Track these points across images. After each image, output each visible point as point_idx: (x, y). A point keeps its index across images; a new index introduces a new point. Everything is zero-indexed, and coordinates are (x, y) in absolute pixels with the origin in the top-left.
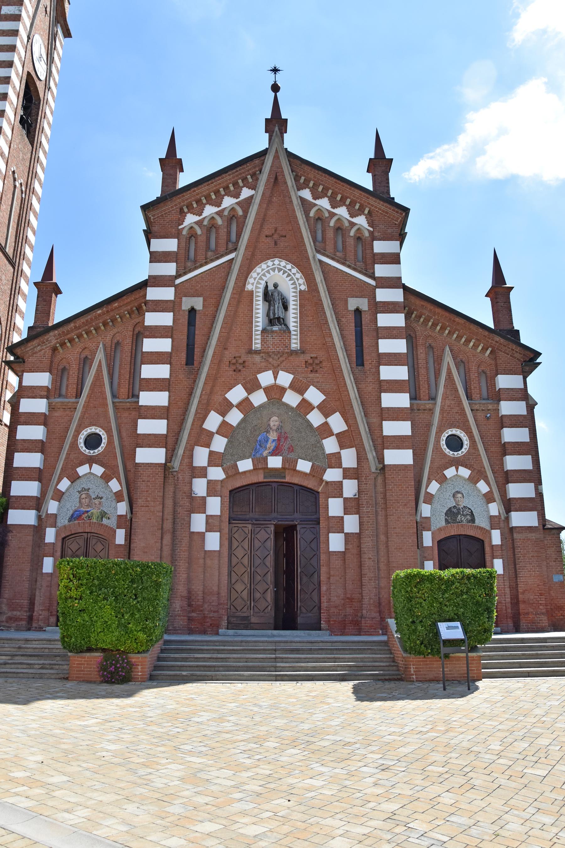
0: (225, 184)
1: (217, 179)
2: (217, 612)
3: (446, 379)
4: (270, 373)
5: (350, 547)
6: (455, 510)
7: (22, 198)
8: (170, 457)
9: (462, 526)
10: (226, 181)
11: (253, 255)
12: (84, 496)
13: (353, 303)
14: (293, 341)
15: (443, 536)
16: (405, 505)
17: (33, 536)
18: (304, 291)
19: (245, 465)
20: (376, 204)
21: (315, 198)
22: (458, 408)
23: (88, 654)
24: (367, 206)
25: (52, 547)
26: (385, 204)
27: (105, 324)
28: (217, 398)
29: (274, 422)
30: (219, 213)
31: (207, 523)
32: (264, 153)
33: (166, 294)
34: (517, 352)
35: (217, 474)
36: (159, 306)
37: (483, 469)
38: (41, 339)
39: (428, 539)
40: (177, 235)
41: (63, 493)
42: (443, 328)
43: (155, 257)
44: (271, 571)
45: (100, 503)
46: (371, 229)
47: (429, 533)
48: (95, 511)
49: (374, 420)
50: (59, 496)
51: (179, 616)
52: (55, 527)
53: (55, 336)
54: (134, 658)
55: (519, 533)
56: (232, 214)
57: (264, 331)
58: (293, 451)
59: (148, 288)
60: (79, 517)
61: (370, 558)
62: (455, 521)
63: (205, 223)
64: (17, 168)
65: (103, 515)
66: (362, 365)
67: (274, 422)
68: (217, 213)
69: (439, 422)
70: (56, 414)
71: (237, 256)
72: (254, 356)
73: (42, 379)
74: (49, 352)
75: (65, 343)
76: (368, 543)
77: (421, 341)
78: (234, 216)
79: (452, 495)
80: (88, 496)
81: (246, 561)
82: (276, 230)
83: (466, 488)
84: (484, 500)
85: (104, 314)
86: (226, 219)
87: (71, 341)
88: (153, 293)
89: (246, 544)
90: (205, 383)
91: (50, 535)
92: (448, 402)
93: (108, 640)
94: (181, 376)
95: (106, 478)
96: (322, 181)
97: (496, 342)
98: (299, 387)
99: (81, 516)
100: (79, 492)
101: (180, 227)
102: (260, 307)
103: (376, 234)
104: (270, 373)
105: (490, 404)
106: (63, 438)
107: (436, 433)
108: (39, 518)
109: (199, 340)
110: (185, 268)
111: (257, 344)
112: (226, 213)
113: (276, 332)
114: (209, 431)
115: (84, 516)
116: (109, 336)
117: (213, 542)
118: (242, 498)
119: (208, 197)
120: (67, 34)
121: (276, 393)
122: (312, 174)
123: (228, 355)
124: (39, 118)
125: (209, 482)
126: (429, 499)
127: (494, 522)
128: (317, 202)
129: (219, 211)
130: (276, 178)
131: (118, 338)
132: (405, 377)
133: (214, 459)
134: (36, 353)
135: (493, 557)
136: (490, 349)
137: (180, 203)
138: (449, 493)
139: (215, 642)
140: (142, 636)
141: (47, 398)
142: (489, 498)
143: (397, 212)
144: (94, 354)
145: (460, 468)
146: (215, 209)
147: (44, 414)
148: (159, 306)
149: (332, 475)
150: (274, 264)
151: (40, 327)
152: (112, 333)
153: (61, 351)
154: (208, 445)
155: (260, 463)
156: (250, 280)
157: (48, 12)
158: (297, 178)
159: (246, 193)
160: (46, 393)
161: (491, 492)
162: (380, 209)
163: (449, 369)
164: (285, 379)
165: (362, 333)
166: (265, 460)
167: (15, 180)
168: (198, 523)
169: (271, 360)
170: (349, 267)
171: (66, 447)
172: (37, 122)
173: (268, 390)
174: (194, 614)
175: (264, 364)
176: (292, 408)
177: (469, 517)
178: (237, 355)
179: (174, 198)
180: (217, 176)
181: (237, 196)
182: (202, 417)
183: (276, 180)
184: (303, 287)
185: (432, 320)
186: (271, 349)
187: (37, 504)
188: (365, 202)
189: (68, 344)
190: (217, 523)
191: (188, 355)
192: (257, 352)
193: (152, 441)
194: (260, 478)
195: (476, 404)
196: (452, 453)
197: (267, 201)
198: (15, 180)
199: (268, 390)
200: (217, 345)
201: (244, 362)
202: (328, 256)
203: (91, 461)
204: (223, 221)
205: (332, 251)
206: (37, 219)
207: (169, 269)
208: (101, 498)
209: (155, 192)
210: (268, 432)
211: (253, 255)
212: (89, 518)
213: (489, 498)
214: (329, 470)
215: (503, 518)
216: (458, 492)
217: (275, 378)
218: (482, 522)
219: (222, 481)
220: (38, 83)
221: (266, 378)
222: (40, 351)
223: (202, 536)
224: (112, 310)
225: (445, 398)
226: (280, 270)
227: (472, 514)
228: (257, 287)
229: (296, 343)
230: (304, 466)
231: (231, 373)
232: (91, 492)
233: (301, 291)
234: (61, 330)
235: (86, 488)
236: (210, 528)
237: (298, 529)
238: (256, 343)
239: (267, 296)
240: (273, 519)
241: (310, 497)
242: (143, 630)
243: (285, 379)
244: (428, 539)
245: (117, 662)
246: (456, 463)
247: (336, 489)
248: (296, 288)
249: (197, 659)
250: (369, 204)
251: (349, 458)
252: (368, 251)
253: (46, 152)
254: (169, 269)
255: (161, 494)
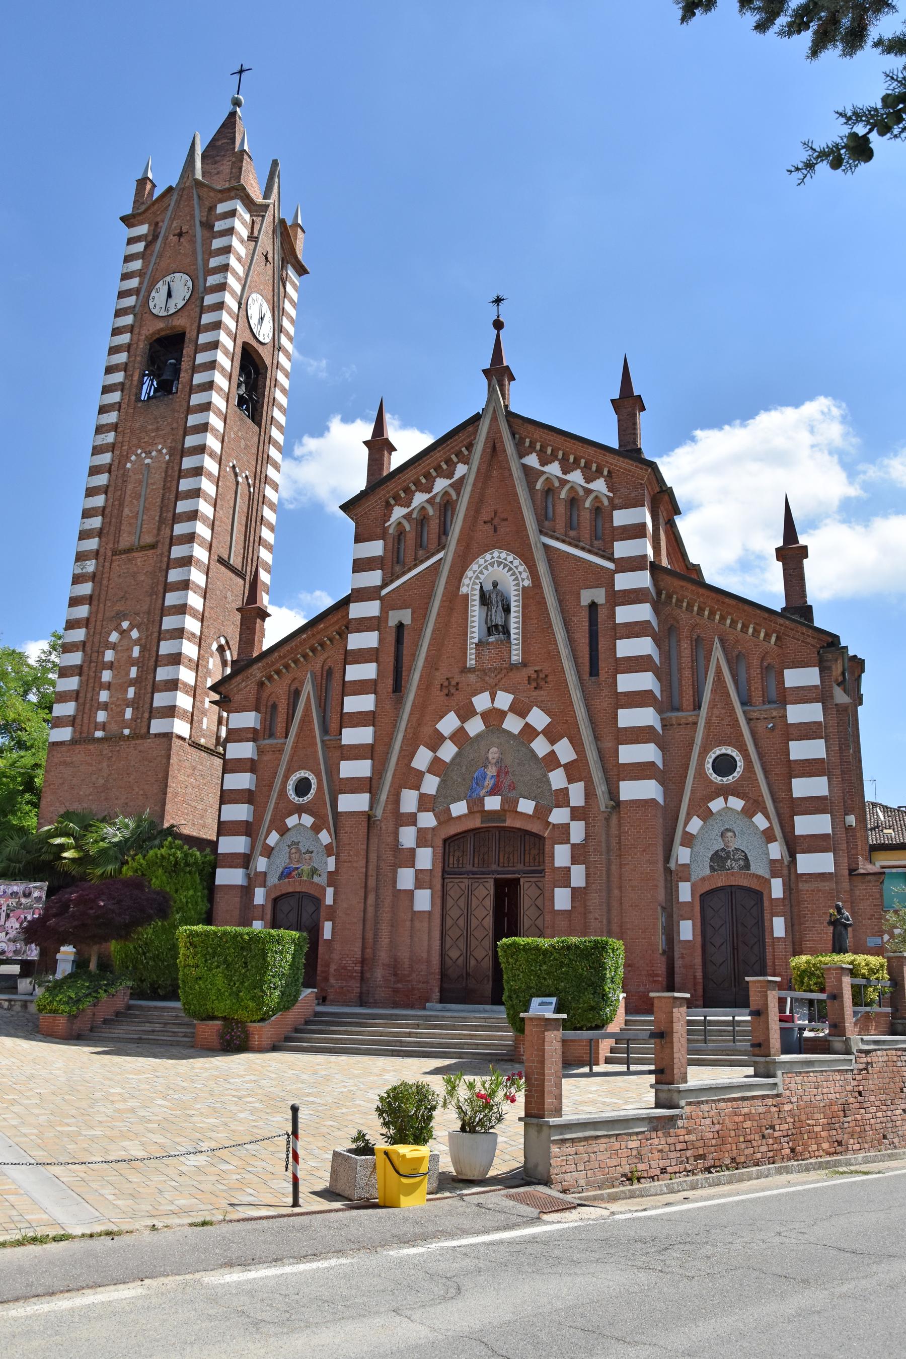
0: (435, 464)
1: (424, 459)
2: (427, 982)
3: (714, 681)
4: (486, 695)
5: (577, 904)
6: (723, 854)
7: (250, 492)
8: (373, 803)
9: (733, 874)
10: (436, 459)
11: (468, 547)
12: (293, 851)
13: (587, 596)
14: (514, 652)
15: (707, 887)
16: (644, 851)
17: (241, 897)
18: (528, 587)
19: (459, 808)
20: (614, 462)
21: (542, 465)
22: (729, 719)
23: (211, 1022)
24: (605, 466)
25: (260, 910)
26: (626, 460)
27: (313, 650)
28: (426, 730)
29: (493, 754)
30: (430, 501)
31: (416, 878)
32: (477, 418)
33: (371, 609)
34: (808, 636)
35: (427, 820)
36: (364, 625)
37: (760, 799)
38: (245, 674)
39: (685, 892)
40: (383, 536)
41: (273, 848)
42: (712, 613)
43: (360, 566)
44: (491, 934)
45: (310, 859)
46: (611, 495)
47: (688, 884)
48: (305, 867)
49: (607, 744)
50: (268, 852)
51: (381, 987)
52: (265, 887)
53: (259, 669)
54: (253, 1027)
55: (806, 881)
56: (446, 498)
57: (480, 644)
58: (514, 788)
59: (351, 605)
60: (289, 875)
61: (596, 919)
62: (723, 868)
63: (414, 516)
64: (238, 460)
65: (314, 871)
66: (597, 675)
67: (493, 754)
68: (428, 501)
69: (703, 738)
70: (265, 758)
71: (446, 555)
72: (469, 675)
73: (248, 719)
74: (254, 688)
75: (272, 676)
76: (595, 900)
77: (685, 633)
78: (448, 501)
79: (719, 834)
80: (298, 850)
81: (461, 922)
82: (496, 513)
83: (738, 825)
84: (764, 839)
85: (309, 638)
86: (437, 507)
87: (278, 672)
88: (357, 610)
89: (462, 902)
90: (411, 714)
91: (260, 896)
92: (716, 712)
93: (222, 1007)
94: (388, 707)
95: (316, 829)
96: (550, 441)
97: (781, 625)
98: (519, 709)
99: (291, 873)
100: (289, 846)
101: (386, 525)
102: (476, 613)
103: (616, 501)
104: (486, 695)
105: (775, 709)
106: (271, 786)
107: (699, 753)
108: (248, 876)
109: (406, 659)
110: (392, 575)
111: (471, 662)
112: (438, 500)
113: (492, 643)
114: (418, 770)
115: (294, 873)
116: (317, 664)
117: (423, 900)
118: (460, 849)
119: (417, 483)
120: (301, 270)
121: (493, 717)
122: (538, 434)
123: (440, 677)
124: (267, 389)
125: (419, 831)
126: (689, 840)
127: (775, 868)
128: (546, 469)
129: (431, 498)
130: (494, 448)
131: (330, 663)
132: (344, 765)
133: (425, 803)
134: (241, 690)
135: (774, 914)
136: (774, 635)
137: (384, 495)
138: (717, 832)
139: (365, 1014)
140: (251, 1004)
141: (254, 740)
142: (769, 836)
143: (641, 469)
144: (302, 683)
145: (731, 798)
146: (425, 497)
147: (252, 760)
148: (364, 625)
149: (559, 816)
150: (493, 558)
151: (243, 660)
152: (322, 658)
153: (269, 685)
154: (417, 787)
155: (476, 805)
156: (466, 581)
157: (270, 259)
158: (519, 444)
159: (461, 470)
160: (251, 736)
161: (770, 829)
162: (621, 468)
163: (718, 667)
164: (504, 700)
165: (597, 631)
166: (481, 801)
167: (236, 475)
168: (406, 878)
169: (487, 678)
170: (583, 549)
171: (274, 795)
172: (264, 395)
173: (485, 716)
174: (399, 985)
175: (479, 684)
176: (515, 735)
177: (742, 863)
178: (450, 676)
179: (377, 491)
180: (425, 456)
181: (450, 475)
182: (409, 754)
183: (494, 449)
184: (527, 583)
185: (697, 604)
186: (487, 665)
187: (245, 861)
188: (602, 460)
189: (276, 677)
190: (427, 879)
191: (396, 680)
192: (471, 670)
193: (354, 785)
194: (477, 823)
195: (754, 711)
196: (719, 778)
197: (484, 476)
198: (236, 475)
199: (485, 716)
200: (424, 667)
201: (457, 684)
202: (557, 539)
203: (300, 810)
204: (434, 511)
205: (563, 531)
206: (296, 290)
207: (374, 578)
208: (312, 852)
209: (358, 483)
210: (485, 767)
211: (468, 547)
212: (300, 875)
213: (769, 836)
214: (555, 810)
215: (786, 863)
216: (728, 830)
217: (493, 700)
218: (759, 868)
219: (433, 829)
220: (260, 349)
221: (481, 702)
222: (245, 688)
223: (410, 893)
224: (318, 633)
225: (712, 706)
226: (499, 564)
227: (746, 859)
228: (473, 589)
229: (517, 655)
230: (526, 806)
231: (443, 698)
232: (301, 846)
233: (524, 587)
234: (264, 661)
235: (296, 841)
236: (420, 884)
237: (522, 883)
238: (471, 659)
239: (485, 600)
240: (493, 872)
241: (532, 843)
242: (253, 998)
243: (504, 700)
244: (685, 892)
245: (233, 1030)
246: (725, 792)
247: (563, 833)
248: (517, 585)
249: (351, 1033)
250: (607, 462)
251: (577, 794)
252: (607, 525)
253: (282, 426)
254: (374, 578)
255: (365, 847)
